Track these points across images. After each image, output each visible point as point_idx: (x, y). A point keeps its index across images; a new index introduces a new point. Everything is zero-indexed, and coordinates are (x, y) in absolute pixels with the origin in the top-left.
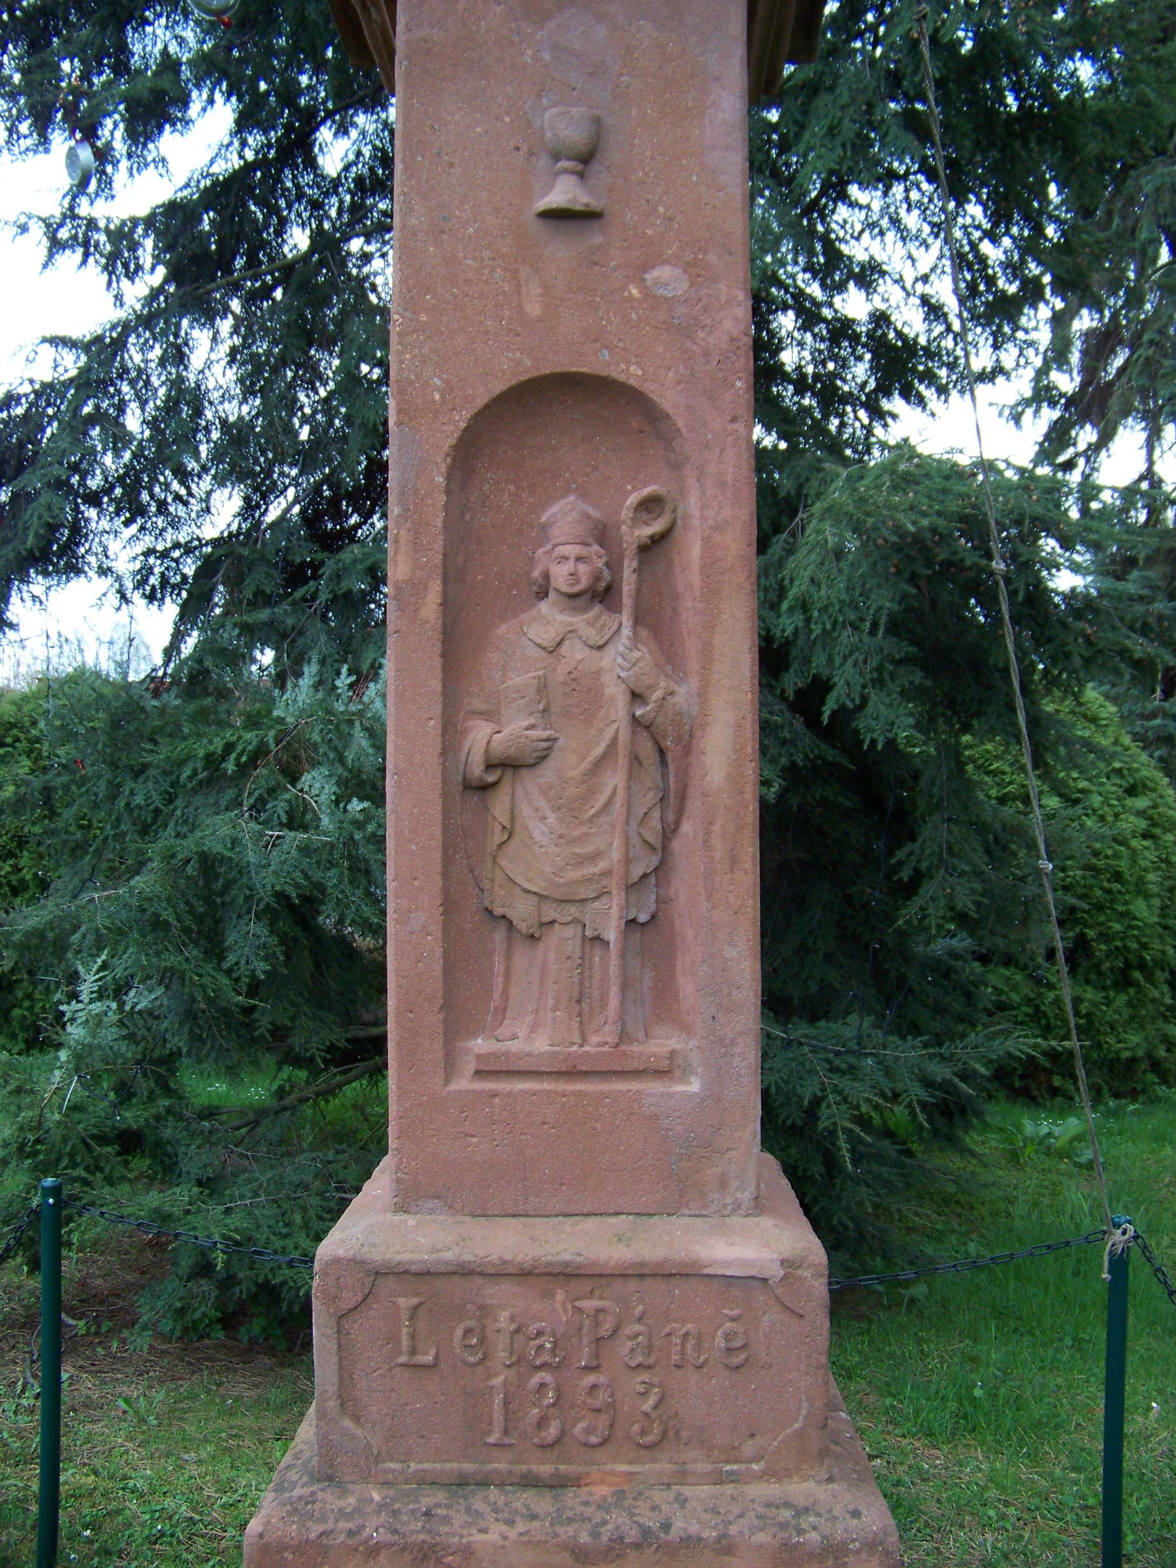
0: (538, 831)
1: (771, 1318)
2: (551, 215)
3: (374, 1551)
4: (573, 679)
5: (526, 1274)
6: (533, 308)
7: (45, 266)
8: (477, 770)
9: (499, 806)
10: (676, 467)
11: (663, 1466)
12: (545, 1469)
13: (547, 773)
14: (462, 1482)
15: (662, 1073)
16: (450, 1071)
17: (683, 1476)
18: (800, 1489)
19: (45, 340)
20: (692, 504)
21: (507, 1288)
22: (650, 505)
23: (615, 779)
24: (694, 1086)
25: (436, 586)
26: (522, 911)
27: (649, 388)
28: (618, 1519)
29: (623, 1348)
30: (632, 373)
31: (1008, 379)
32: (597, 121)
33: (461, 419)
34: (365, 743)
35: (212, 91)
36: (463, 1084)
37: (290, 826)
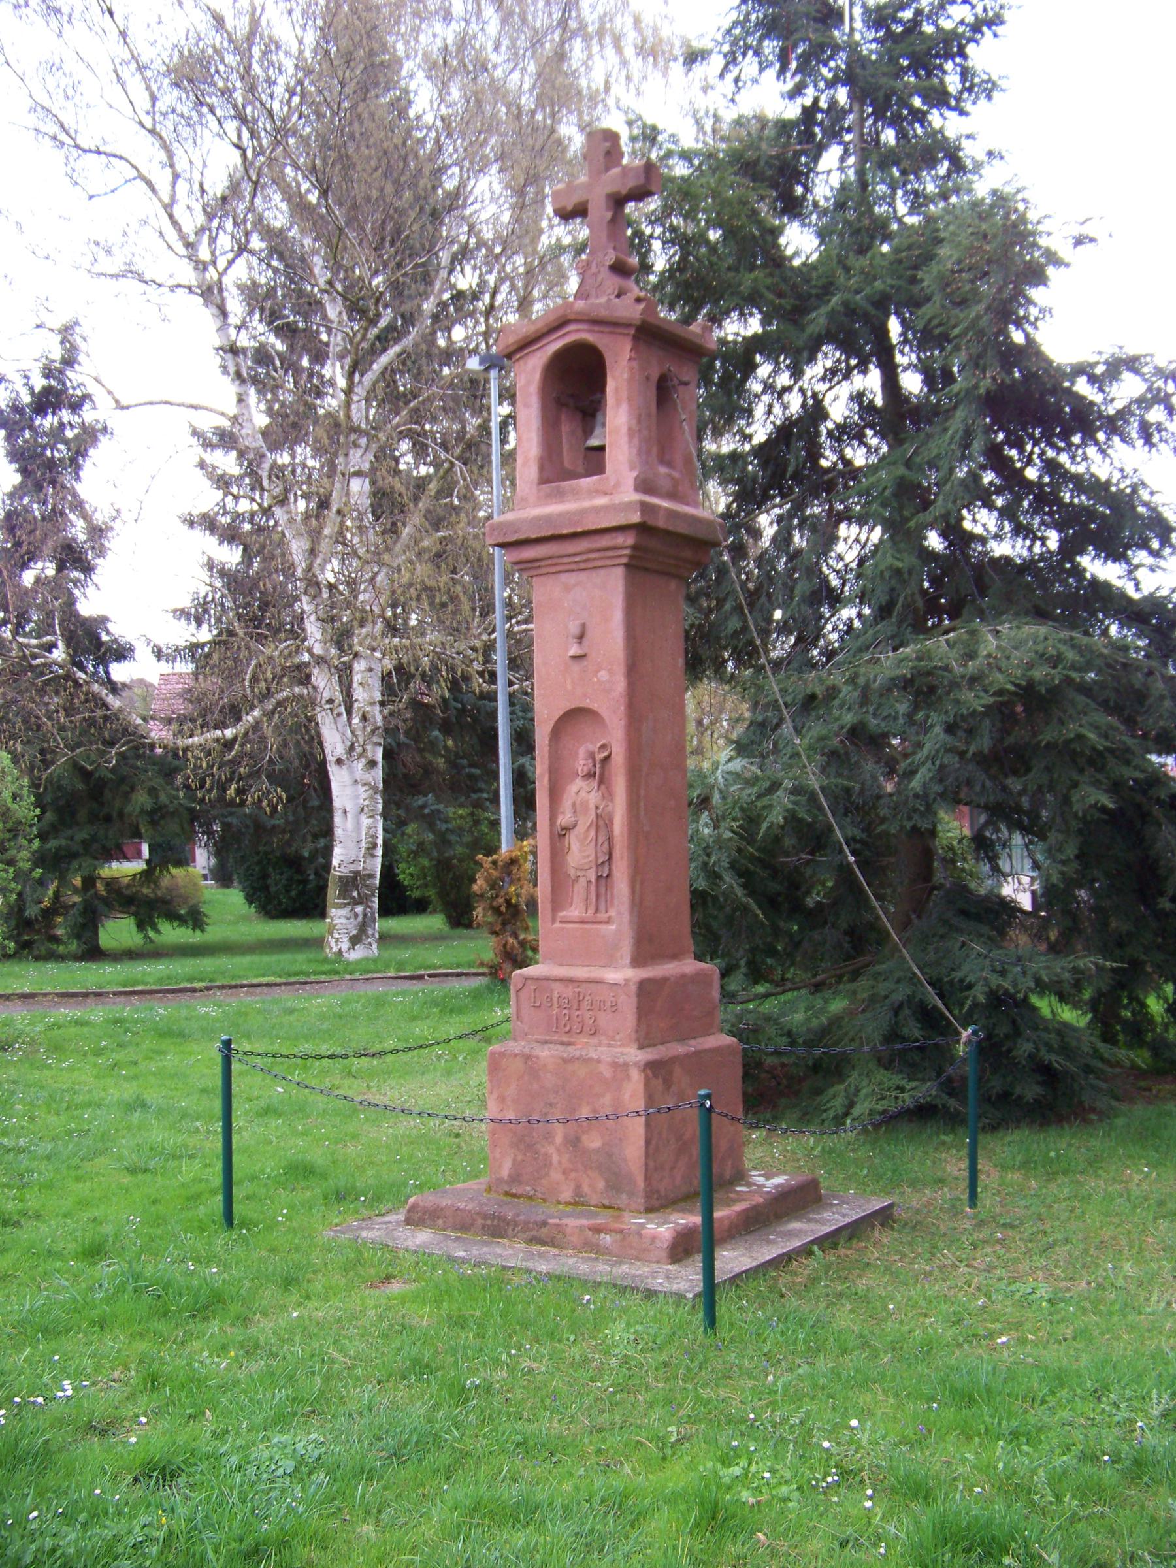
2: (574, 657)
3: (516, 1055)
5: (561, 980)
6: (569, 687)
7: (1092, 240)
14: (546, 1042)
16: (553, 921)
17: (600, 1045)
19: (584, 626)
22: (603, 747)
24: (613, 927)
27: (600, 711)
30: (594, 706)
33: (552, 723)
36: (557, 925)
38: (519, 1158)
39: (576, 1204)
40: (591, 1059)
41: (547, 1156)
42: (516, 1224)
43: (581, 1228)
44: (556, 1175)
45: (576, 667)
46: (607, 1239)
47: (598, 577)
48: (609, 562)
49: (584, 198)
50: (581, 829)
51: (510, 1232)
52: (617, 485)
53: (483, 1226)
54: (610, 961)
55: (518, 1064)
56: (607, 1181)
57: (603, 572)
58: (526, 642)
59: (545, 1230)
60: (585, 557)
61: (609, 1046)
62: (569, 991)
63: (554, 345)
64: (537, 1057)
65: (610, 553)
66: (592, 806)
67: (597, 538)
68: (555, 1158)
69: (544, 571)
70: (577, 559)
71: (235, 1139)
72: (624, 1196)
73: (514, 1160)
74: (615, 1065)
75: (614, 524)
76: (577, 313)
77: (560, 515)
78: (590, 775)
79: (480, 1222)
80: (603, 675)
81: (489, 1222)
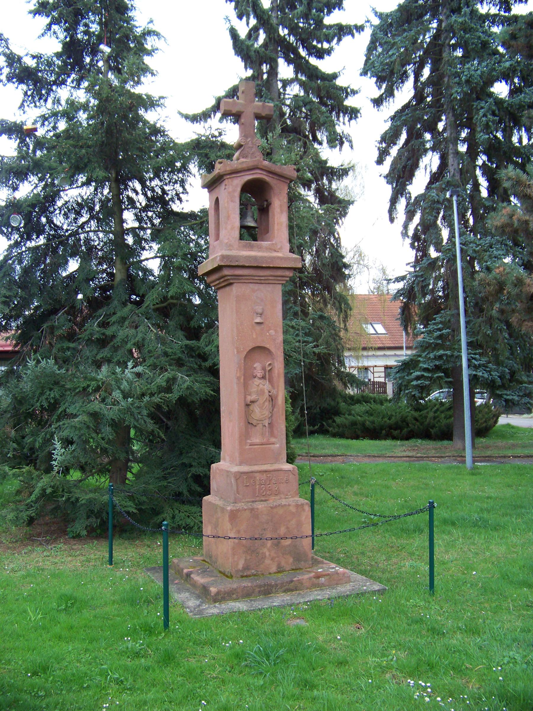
0: (257, 411)
1: (291, 476)
3: (246, 510)
4: (261, 390)
5: (260, 472)
6: (254, 336)
8: (249, 403)
9: (251, 408)
10: (273, 359)
11: (279, 497)
12: (263, 499)
13: (258, 403)
15: (273, 444)
17: (281, 498)
18: (296, 499)
20: (276, 364)
21: (257, 474)
22: (270, 364)
23: (267, 404)
24: (278, 445)
25: (243, 377)
26: (254, 422)
27: (270, 348)
28: (275, 504)
29: (273, 481)
30: (267, 346)
31: (30, 12)
32: (263, 309)
34: (126, 384)
35: (144, 260)
37: (114, 405)
38: (248, 557)
39: (279, 572)
40: (285, 505)
41: (264, 554)
42: (277, 585)
43: (310, 578)
44: (268, 562)
45: (258, 328)
46: (322, 580)
47: (269, 288)
48: (259, 281)
49: (242, 110)
50: (261, 401)
51: (274, 590)
52: (281, 248)
53: (259, 592)
54: (277, 460)
55: (247, 514)
56: (294, 558)
57: (271, 285)
58: (290, 315)
59: (292, 584)
60: (266, 278)
61: (285, 498)
62: (264, 476)
63: (248, 177)
64: (258, 509)
65: (279, 278)
66: (266, 392)
67: (275, 270)
68: (267, 554)
69: (243, 281)
70: (263, 278)
71: (427, 544)
72: (302, 563)
73: (246, 560)
74: (297, 506)
75: (286, 266)
76: (265, 167)
77: (262, 257)
78: (264, 377)
79: (257, 590)
80: (272, 332)
81: (262, 589)
